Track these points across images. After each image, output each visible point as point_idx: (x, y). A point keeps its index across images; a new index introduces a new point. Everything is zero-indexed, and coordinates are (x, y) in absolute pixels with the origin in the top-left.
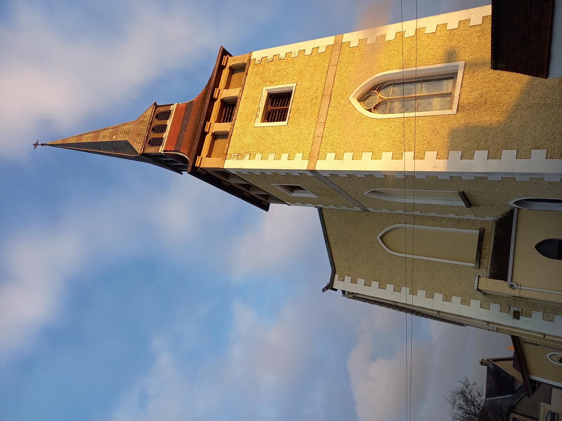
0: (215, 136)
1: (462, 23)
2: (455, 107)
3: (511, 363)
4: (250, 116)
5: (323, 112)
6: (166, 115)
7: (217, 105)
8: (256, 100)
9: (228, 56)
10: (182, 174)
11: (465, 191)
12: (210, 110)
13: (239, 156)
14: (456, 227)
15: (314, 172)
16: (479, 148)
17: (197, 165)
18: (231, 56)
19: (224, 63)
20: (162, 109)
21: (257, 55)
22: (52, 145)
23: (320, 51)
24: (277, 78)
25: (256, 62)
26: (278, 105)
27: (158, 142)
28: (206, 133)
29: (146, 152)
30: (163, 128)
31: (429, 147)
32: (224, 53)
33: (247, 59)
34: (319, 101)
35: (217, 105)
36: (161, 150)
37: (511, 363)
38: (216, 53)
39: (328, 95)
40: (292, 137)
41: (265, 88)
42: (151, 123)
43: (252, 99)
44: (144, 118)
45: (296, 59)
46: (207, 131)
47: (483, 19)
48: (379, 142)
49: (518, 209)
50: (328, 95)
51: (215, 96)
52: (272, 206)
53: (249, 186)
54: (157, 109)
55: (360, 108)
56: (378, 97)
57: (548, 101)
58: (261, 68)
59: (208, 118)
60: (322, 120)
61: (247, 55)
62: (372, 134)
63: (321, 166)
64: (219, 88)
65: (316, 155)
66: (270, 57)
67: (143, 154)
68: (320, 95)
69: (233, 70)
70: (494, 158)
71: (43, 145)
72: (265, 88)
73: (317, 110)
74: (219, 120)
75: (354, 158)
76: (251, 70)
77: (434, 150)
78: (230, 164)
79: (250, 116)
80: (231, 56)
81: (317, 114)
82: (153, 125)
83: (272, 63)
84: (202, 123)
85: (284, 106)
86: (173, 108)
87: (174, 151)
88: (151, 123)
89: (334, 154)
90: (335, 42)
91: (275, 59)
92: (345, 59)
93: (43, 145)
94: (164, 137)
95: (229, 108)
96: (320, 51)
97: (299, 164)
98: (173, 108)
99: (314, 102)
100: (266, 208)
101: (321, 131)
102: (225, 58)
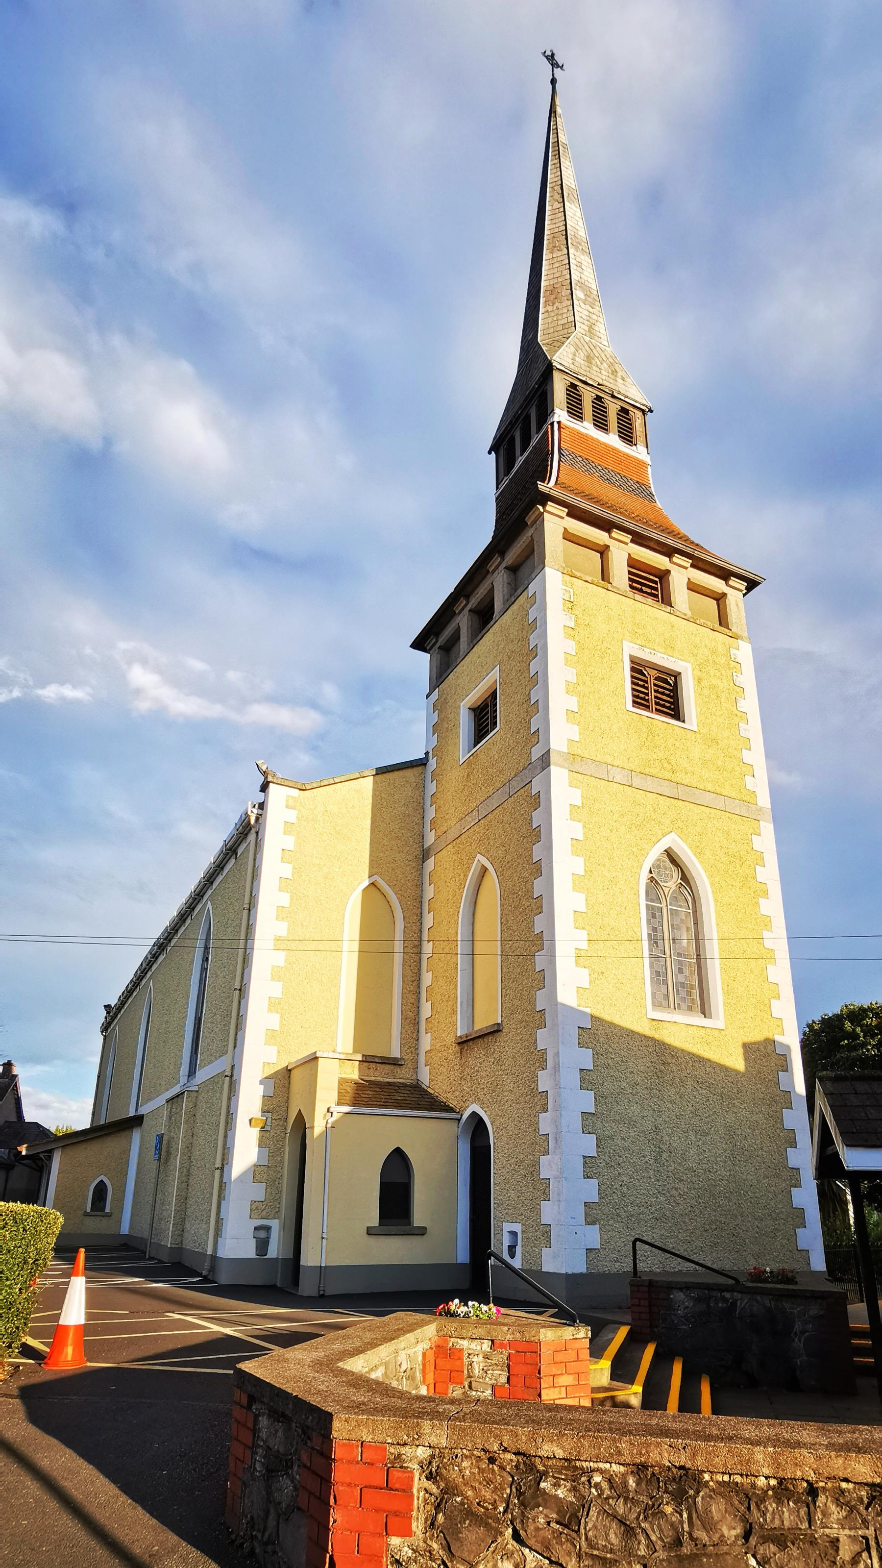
0: (603, 551)
1: (779, 1023)
2: (658, 1015)
3: (13, 1118)
4: (641, 631)
5: (650, 784)
6: (627, 436)
7: (659, 561)
8: (669, 647)
9: (745, 591)
10: (490, 453)
11: (503, 1034)
12: (651, 544)
13: (570, 605)
14: (404, 1018)
15: (545, 761)
16: (596, 1055)
17: (550, 506)
18: (744, 595)
19: (733, 581)
20: (638, 424)
21: (744, 652)
22: (552, 111)
23: (748, 779)
24: (706, 692)
25: (733, 651)
26: (659, 692)
27: (575, 409)
28: (609, 531)
29: (556, 375)
30: (601, 423)
31: (596, 976)
32: (752, 584)
33: (739, 633)
34: (668, 775)
35: (659, 561)
36: (560, 414)
37: (13, 1118)
38: (751, 568)
39: (678, 793)
40: (607, 720)
41: (689, 666)
42: (613, 396)
43: (672, 636)
44: (623, 379)
45: (737, 732)
46: (731, 583)
47: (782, 1055)
48: (601, 887)
49: (459, 1120)
50: (678, 793)
51: (677, 558)
52: (423, 659)
53: (485, 616)
54: (639, 414)
55: (656, 853)
56: (672, 883)
57: (665, 1155)
58: (723, 661)
59: (639, 539)
60: (637, 782)
61: (745, 634)
62: (614, 874)
63: (558, 774)
64: (691, 569)
65: (577, 768)
66: (740, 680)
67: (549, 369)
68: (678, 777)
69: (720, 599)
70: (582, 1079)
71: (553, 81)
72: (689, 666)
73: (653, 771)
74: (632, 563)
75: (574, 841)
76: (720, 638)
77: (591, 982)
78: (554, 583)
79: (641, 631)
80: (744, 595)
81: (647, 771)
82: (607, 398)
83: (732, 684)
84: (631, 527)
85: (656, 703)
86: (639, 452)
87: (560, 448)
88: (613, 396)
89: (580, 804)
90: (761, 809)
91: (738, 689)
92: (734, 826)
93: (553, 81)
94: (585, 424)
95: (650, 584)
96: (748, 779)
97: (561, 734)
98: (639, 452)
99: (666, 765)
100: (419, 644)
101: (618, 779)
102: (743, 585)
